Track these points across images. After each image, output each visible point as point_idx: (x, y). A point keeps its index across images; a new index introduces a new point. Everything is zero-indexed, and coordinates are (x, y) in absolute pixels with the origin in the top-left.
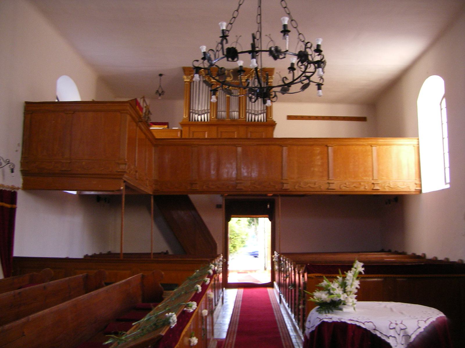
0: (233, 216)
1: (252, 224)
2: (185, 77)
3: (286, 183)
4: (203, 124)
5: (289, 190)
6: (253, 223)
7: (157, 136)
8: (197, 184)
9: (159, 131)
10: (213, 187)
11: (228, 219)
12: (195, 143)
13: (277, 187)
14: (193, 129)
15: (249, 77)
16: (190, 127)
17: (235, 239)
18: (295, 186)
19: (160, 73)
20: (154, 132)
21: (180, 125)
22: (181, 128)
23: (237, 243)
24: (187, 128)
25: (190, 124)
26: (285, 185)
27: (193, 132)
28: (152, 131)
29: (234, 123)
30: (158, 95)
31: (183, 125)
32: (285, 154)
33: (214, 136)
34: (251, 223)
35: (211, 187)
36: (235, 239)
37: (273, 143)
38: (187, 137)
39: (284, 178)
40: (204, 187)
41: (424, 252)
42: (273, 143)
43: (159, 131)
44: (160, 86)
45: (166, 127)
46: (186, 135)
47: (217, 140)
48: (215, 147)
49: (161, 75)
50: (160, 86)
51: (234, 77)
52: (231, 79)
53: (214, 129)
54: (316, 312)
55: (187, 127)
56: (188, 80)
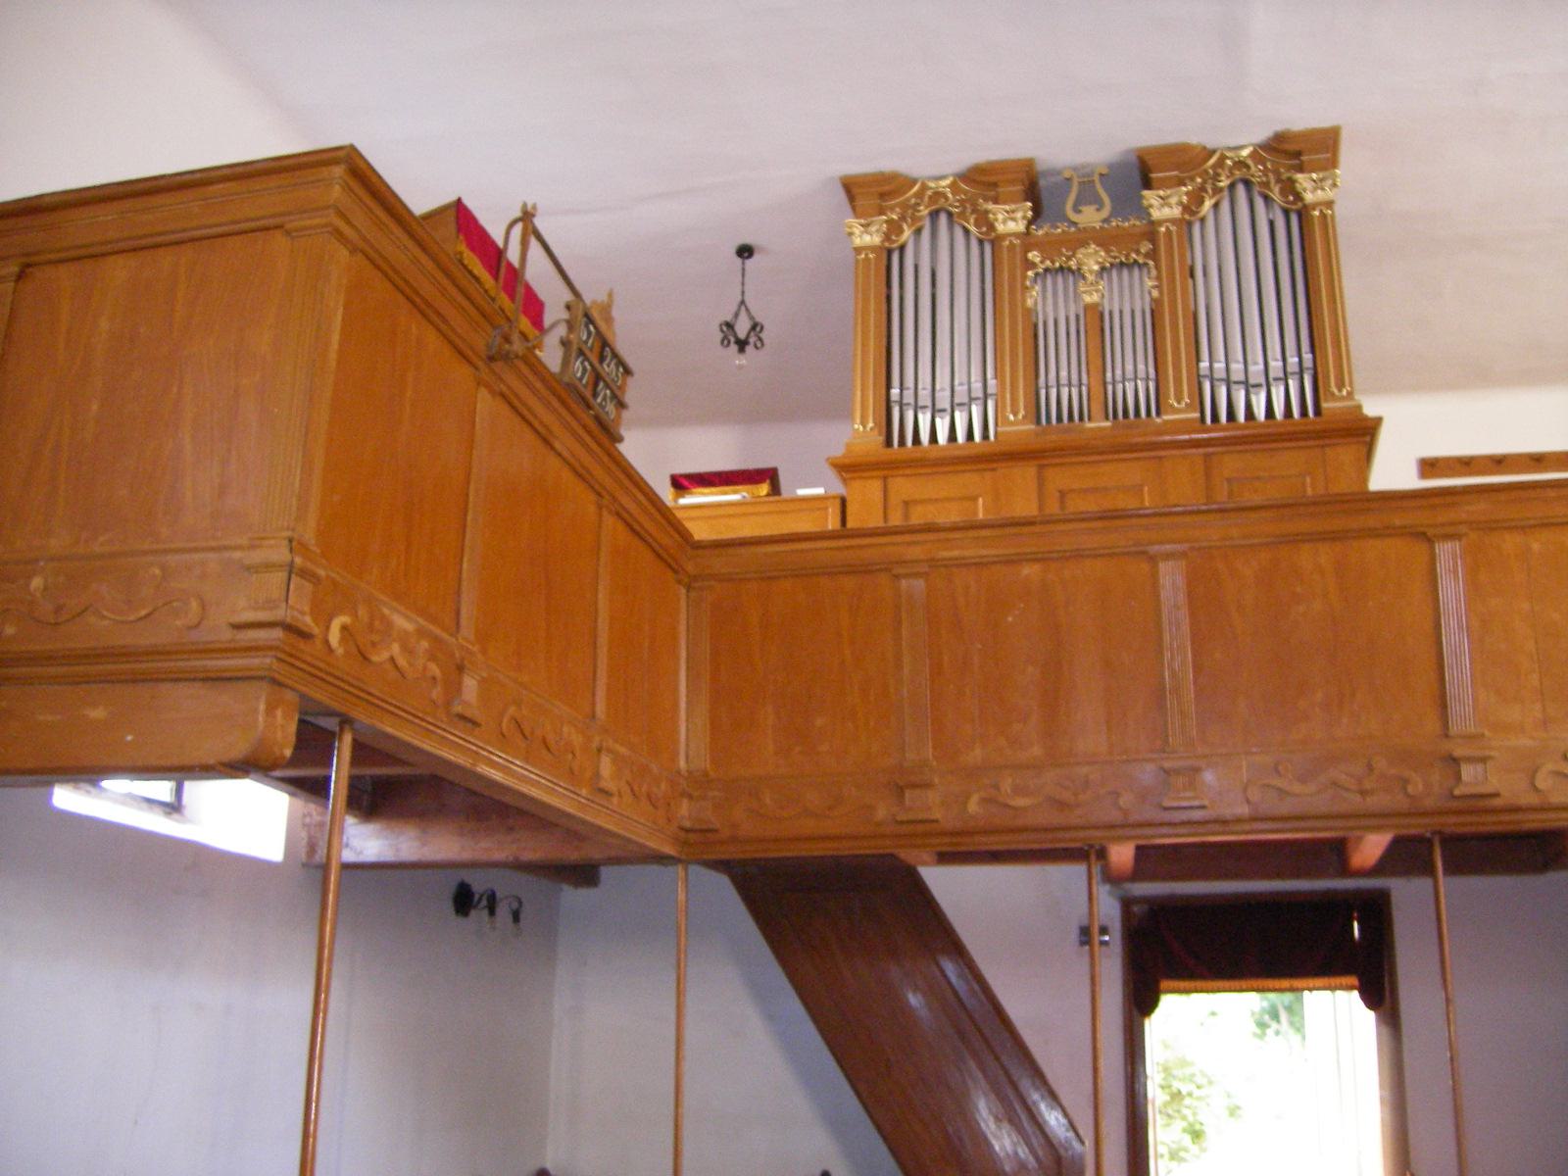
0: (1164, 984)
1: (1268, 1031)
2: (855, 224)
3: (1470, 760)
4: (965, 453)
5: (1497, 802)
6: (1274, 1025)
7: (700, 532)
8: (928, 786)
9: (720, 512)
10: (1021, 802)
11: (1141, 1001)
12: (915, 552)
13: (1417, 786)
14: (903, 487)
15: (1197, 198)
16: (885, 478)
17: (1199, 1098)
18: (1533, 774)
19: (747, 240)
20: (692, 519)
21: (831, 475)
22: (839, 489)
23: (1209, 1112)
24: (874, 487)
25: (892, 458)
26: (1468, 772)
27: (906, 503)
28: (679, 514)
29: (1133, 441)
30: (734, 348)
31: (848, 468)
32: (1451, 591)
33: (1024, 506)
34: (1268, 1027)
35: (1013, 803)
36: (1199, 1098)
37: (1371, 521)
38: (875, 521)
39: (1453, 730)
40: (973, 806)
41: (461, 920)
42: (1371, 521)
43: (720, 512)
44: (743, 302)
45: (764, 489)
46: (866, 513)
47: (1037, 529)
48: (1028, 570)
49: (745, 252)
50: (743, 302)
51: (1114, 208)
52: (1105, 213)
53: (1024, 475)
54: (525, 205)
55: (872, 478)
56: (877, 240)
